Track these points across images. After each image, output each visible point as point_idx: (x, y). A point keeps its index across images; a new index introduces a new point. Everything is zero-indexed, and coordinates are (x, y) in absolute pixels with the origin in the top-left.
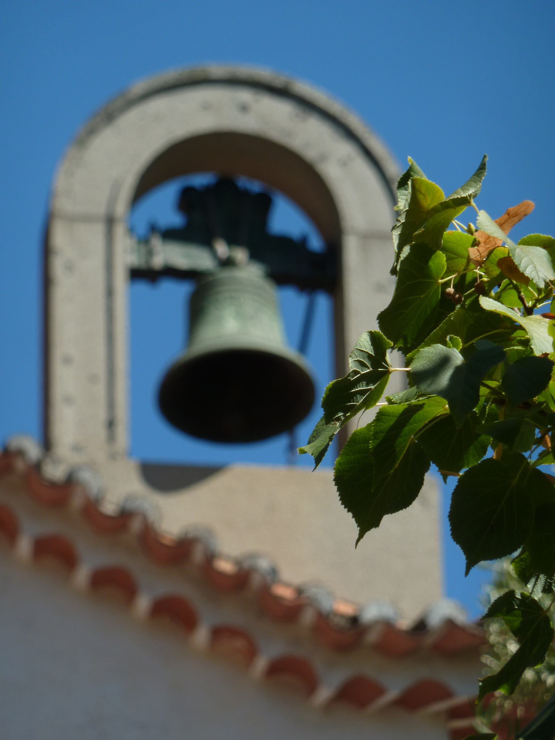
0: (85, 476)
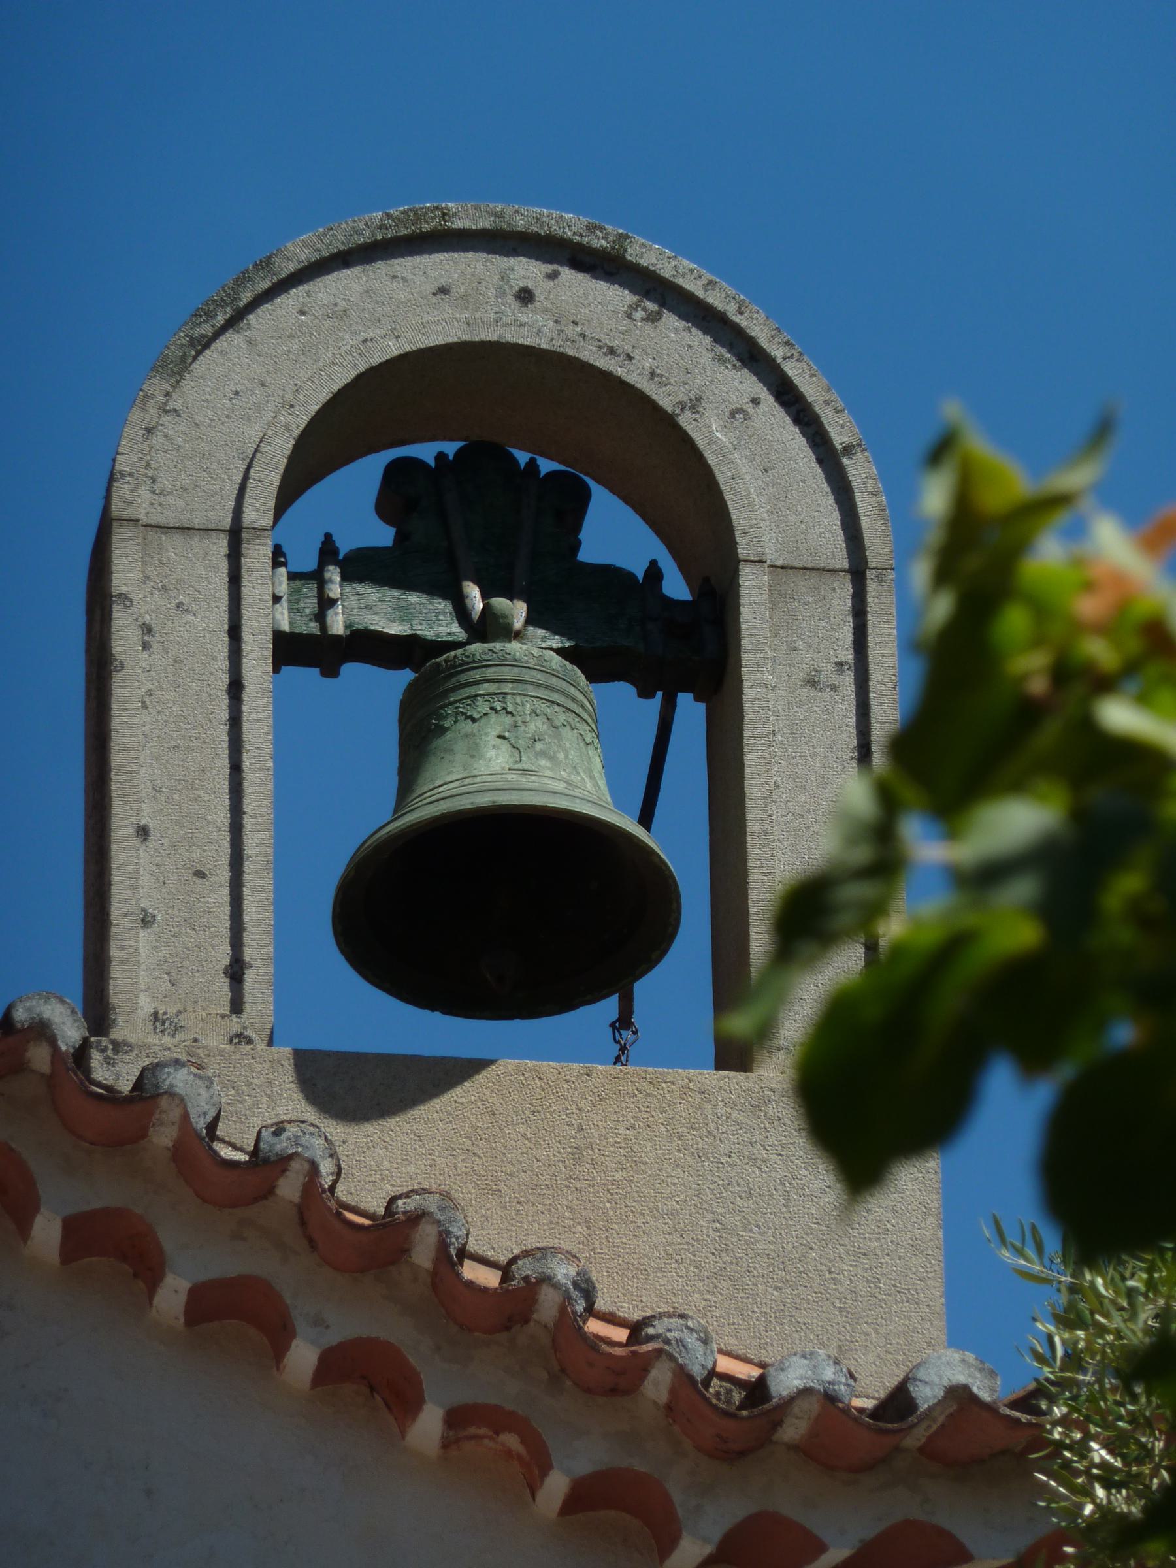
0: (180, 1080)
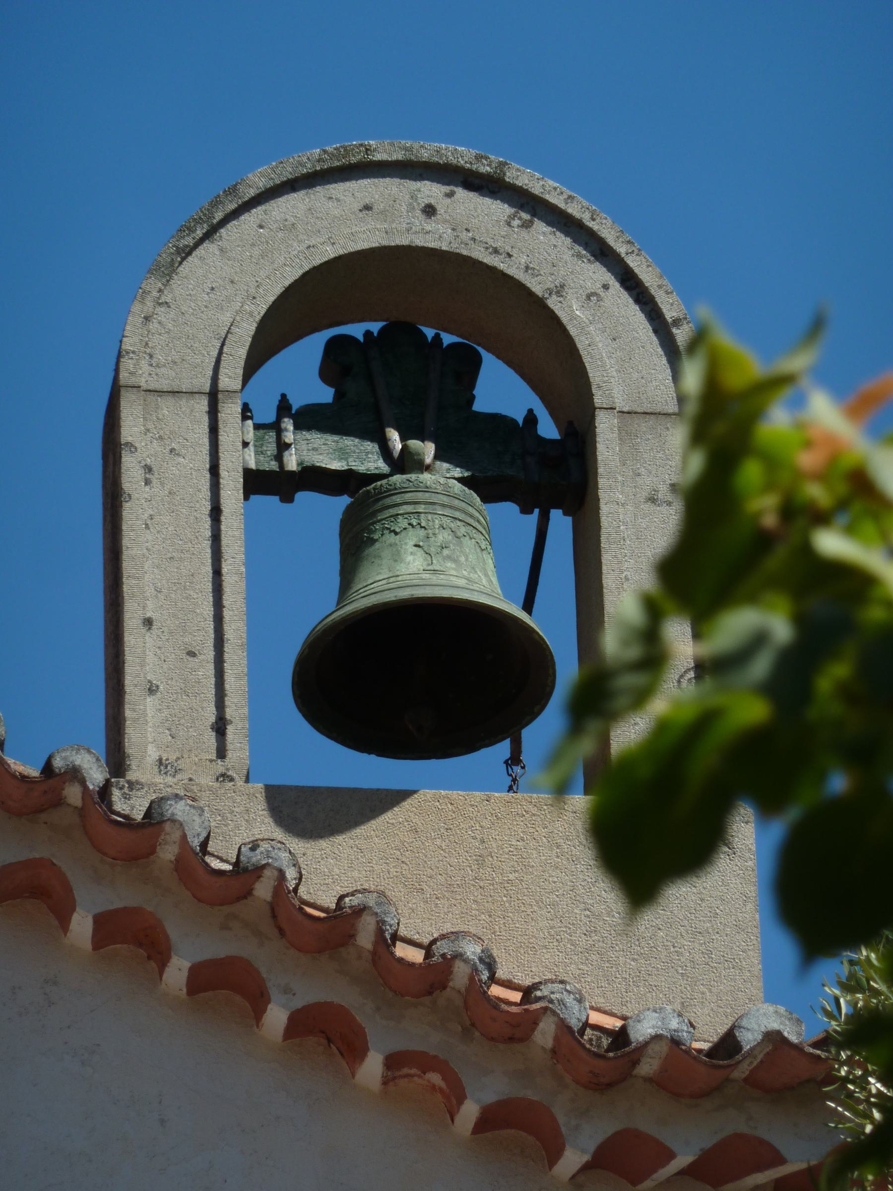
0: (179, 810)
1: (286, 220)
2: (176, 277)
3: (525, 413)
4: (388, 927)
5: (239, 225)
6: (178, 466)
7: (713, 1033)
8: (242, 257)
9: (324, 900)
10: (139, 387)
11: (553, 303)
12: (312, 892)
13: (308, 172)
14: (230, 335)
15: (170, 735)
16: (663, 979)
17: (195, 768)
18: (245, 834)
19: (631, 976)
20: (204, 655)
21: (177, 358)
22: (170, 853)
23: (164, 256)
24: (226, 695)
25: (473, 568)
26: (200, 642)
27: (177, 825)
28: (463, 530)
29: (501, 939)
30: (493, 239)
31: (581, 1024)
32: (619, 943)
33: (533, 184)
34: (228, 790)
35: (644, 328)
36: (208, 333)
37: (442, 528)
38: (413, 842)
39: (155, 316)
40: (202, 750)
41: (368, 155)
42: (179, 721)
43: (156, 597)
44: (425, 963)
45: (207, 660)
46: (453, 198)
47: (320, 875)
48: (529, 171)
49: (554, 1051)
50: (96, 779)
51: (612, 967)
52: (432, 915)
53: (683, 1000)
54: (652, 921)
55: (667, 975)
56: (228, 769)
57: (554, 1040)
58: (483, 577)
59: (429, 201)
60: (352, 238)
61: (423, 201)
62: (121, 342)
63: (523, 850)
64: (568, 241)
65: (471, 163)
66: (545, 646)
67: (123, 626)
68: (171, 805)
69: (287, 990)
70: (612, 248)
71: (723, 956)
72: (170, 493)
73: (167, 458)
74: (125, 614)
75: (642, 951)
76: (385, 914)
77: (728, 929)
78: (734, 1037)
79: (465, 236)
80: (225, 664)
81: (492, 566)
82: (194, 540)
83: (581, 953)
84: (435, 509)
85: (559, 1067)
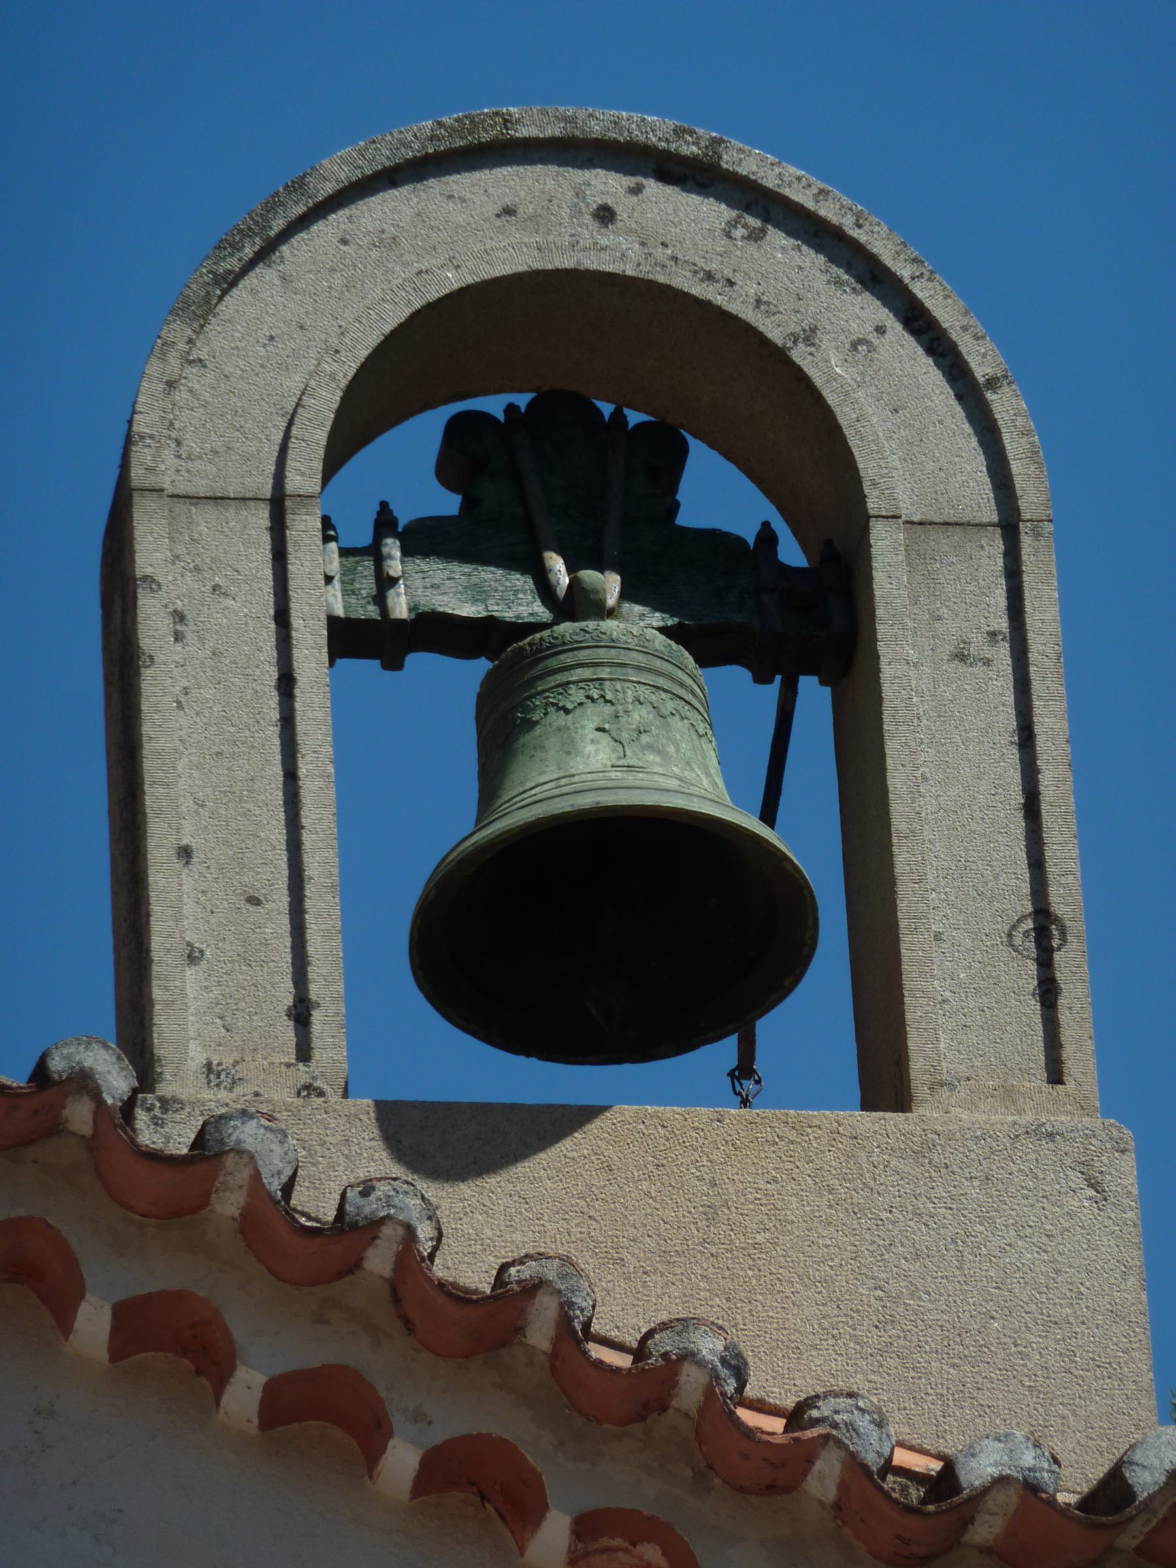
0: (248, 1134)
1: (383, 231)
2: (213, 321)
3: (757, 528)
4: (578, 1312)
5: (309, 240)
6: (226, 612)
7: (1081, 1479)
8: (316, 289)
9: (469, 1277)
10: (162, 490)
11: (799, 355)
12: (450, 1265)
13: (415, 157)
14: (300, 410)
15: (224, 1026)
16: (1001, 1396)
17: (262, 1076)
18: (345, 1177)
19: (950, 1392)
20: (274, 902)
21: (219, 445)
22: (232, 1204)
23: (194, 286)
24: (309, 963)
25: (688, 763)
26: (267, 883)
27: (246, 1159)
28: (670, 705)
29: (746, 1335)
30: (704, 258)
31: (883, 1461)
32: (929, 1339)
33: (765, 172)
34: (317, 1109)
35: (941, 393)
36: (266, 407)
37: (637, 703)
38: (605, 1186)
39: (183, 381)
40: (273, 1049)
41: (507, 129)
42: (236, 1004)
43: (198, 814)
44: (637, 1368)
45: (278, 910)
46: (640, 196)
47: (463, 1238)
48: (757, 152)
49: (838, 1506)
50: (117, 1089)
51: (920, 1378)
52: (638, 1299)
53: (1032, 1428)
54: (981, 1305)
55: (1006, 1389)
56: (314, 1078)
57: (838, 1489)
58: (703, 777)
59: (604, 201)
60: (487, 258)
61: (595, 201)
62: (130, 422)
63: (776, 1197)
64: (821, 259)
65: (668, 141)
66: (801, 881)
67: (146, 859)
68: (235, 1127)
69: (419, 1417)
70: (889, 269)
71: (1093, 1359)
72: (214, 654)
73: (208, 599)
74: (149, 840)
75: (966, 1352)
76: (573, 1292)
77: (1100, 1318)
78: (1123, 1478)
79: (660, 254)
80: (307, 916)
81: (715, 761)
82: (254, 726)
83: (871, 1355)
84: (627, 674)
85: (847, 1531)
